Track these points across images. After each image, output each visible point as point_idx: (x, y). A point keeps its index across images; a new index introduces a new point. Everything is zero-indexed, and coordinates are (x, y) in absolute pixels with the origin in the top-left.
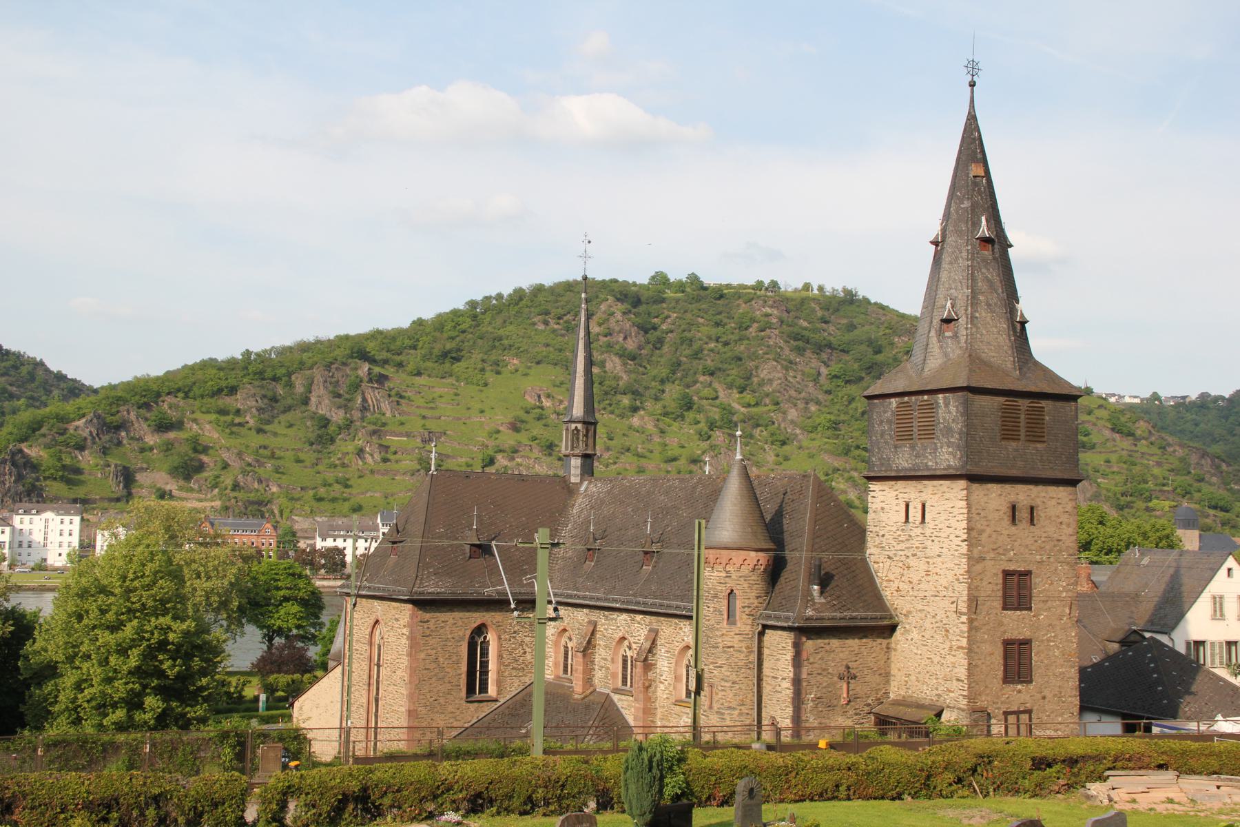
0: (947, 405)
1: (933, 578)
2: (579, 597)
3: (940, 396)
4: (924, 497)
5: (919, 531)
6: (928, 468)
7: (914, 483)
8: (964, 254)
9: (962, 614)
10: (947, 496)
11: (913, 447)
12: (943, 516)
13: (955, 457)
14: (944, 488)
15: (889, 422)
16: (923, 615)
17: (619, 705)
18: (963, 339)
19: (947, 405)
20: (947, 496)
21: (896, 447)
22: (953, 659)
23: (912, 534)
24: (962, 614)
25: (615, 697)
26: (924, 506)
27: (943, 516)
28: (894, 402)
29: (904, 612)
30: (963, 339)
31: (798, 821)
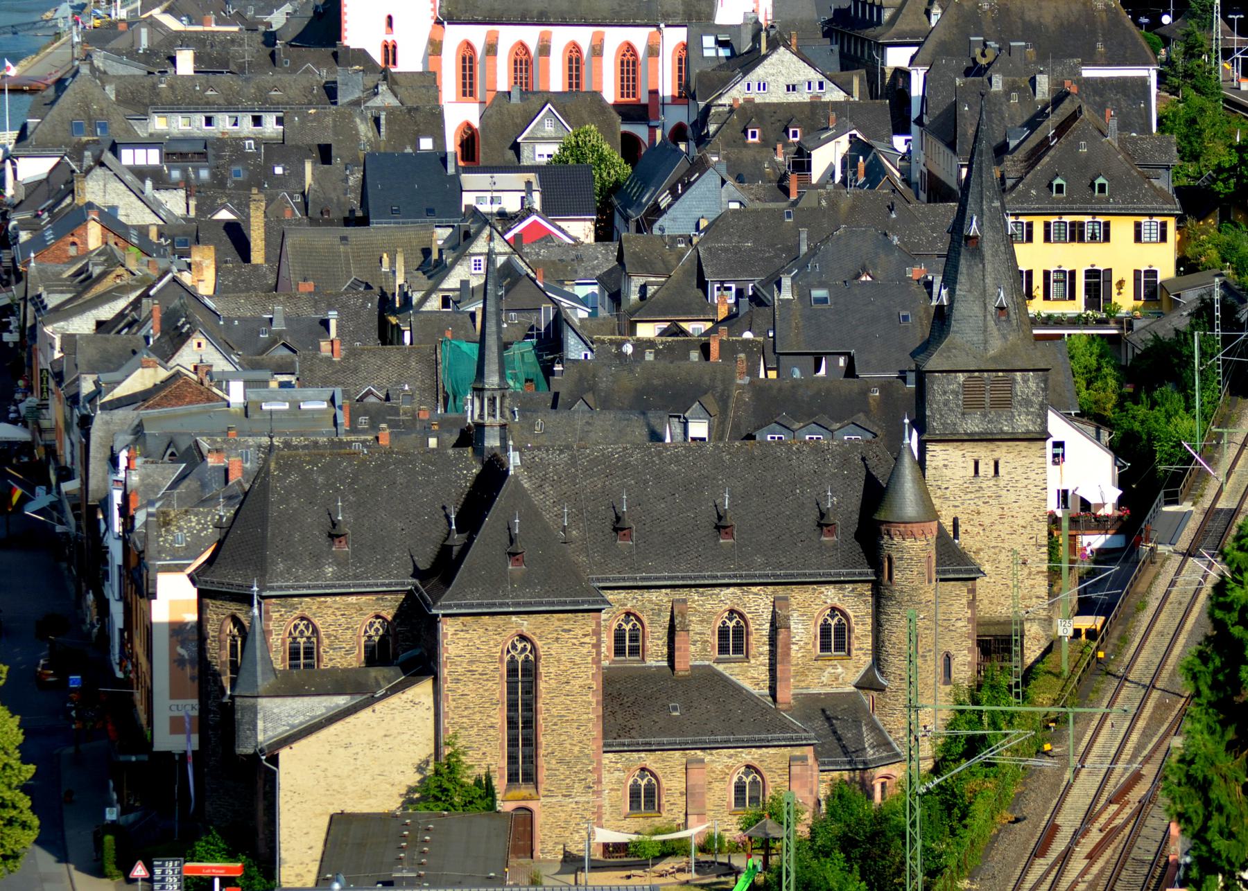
0: (1026, 381)
1: (1007, 520)
2: (304, 587)
3: (1018, 374)
4: (996, 455)
5: (992, 483)
6: (1002, 432)
7: (985, 444)
8: (1002, 248)
9: (1041, 546)
10: (1024, 454)
11: (985, 416)
12: (1020, 471)
13: (1034, 423)
14: (1018, 448)
15: (956, 393)
16: (997, 550)
17: (727, 673)
18: (1014, 322)
19: (1026, 381)
20: (1024, 454)
21: (963, 414)
22: (1032, 582)
23: (984, 485)
24: (1041, 546)
25: (720, 668)
26: (976, 463)
27: (1020, 471)
28: (961, 377)
29: (974, 549)
30: (1014, 322)
31: (526, 881)
